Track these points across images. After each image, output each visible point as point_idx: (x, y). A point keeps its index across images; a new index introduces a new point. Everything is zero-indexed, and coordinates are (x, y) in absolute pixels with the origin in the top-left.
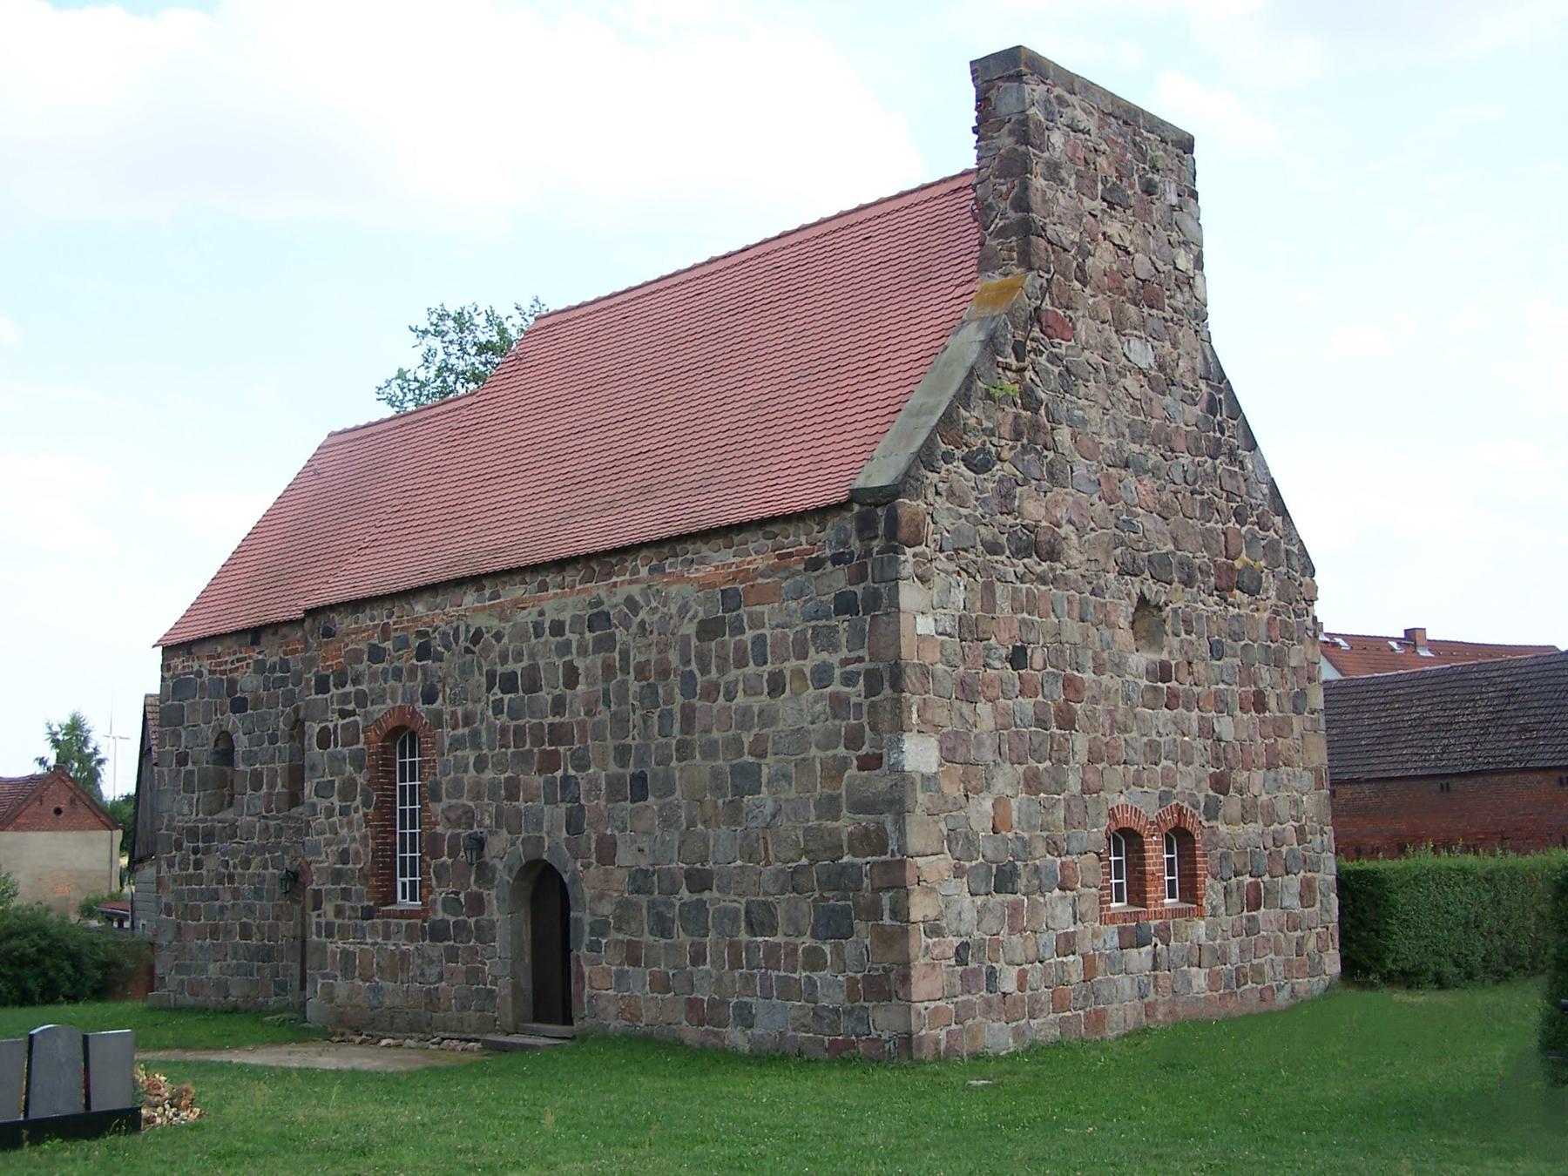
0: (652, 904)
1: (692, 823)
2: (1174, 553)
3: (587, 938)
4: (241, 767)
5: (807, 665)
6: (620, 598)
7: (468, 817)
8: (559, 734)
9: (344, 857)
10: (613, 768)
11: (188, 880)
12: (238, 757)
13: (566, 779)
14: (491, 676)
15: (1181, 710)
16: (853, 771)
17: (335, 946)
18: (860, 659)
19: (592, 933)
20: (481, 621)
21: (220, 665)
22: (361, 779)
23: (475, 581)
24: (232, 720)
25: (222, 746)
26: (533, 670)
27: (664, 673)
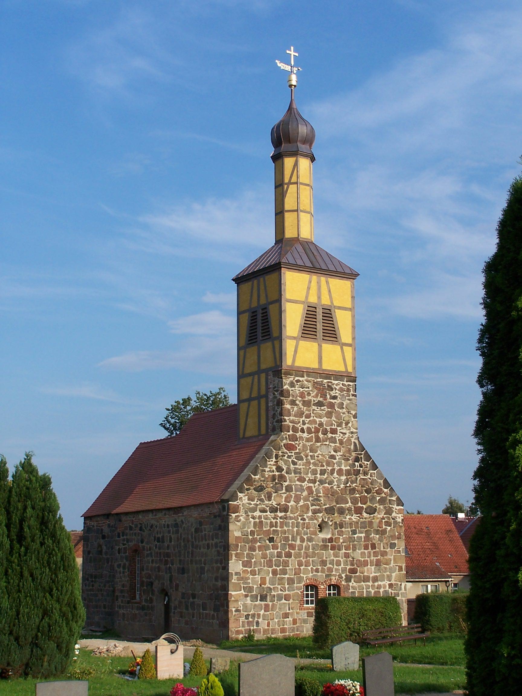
0: (185, 602)
1: (193, 581)
2: (335, 506)
3: (173, 610)
4: (104, 556)
5: (214, 542)
6: (180, 520)
7: (149, 576)
8: (168, 555)
9: (123, 586)
10: (178, 565)
11: (91, 590)
12: (103, 553)
13: (170, 567)
14: (155, 537)
15: (337, 551)
16: (221, 570)
17: (121, 611)
18: (222, 542)
19: (174, 609)
20: (153, 522)
21: (99, 524)
22: (127, 564)
23: (152, 511)
24: (102, 541)
25: (100, 549)
26: (163, 537)
27: (188, 541)
